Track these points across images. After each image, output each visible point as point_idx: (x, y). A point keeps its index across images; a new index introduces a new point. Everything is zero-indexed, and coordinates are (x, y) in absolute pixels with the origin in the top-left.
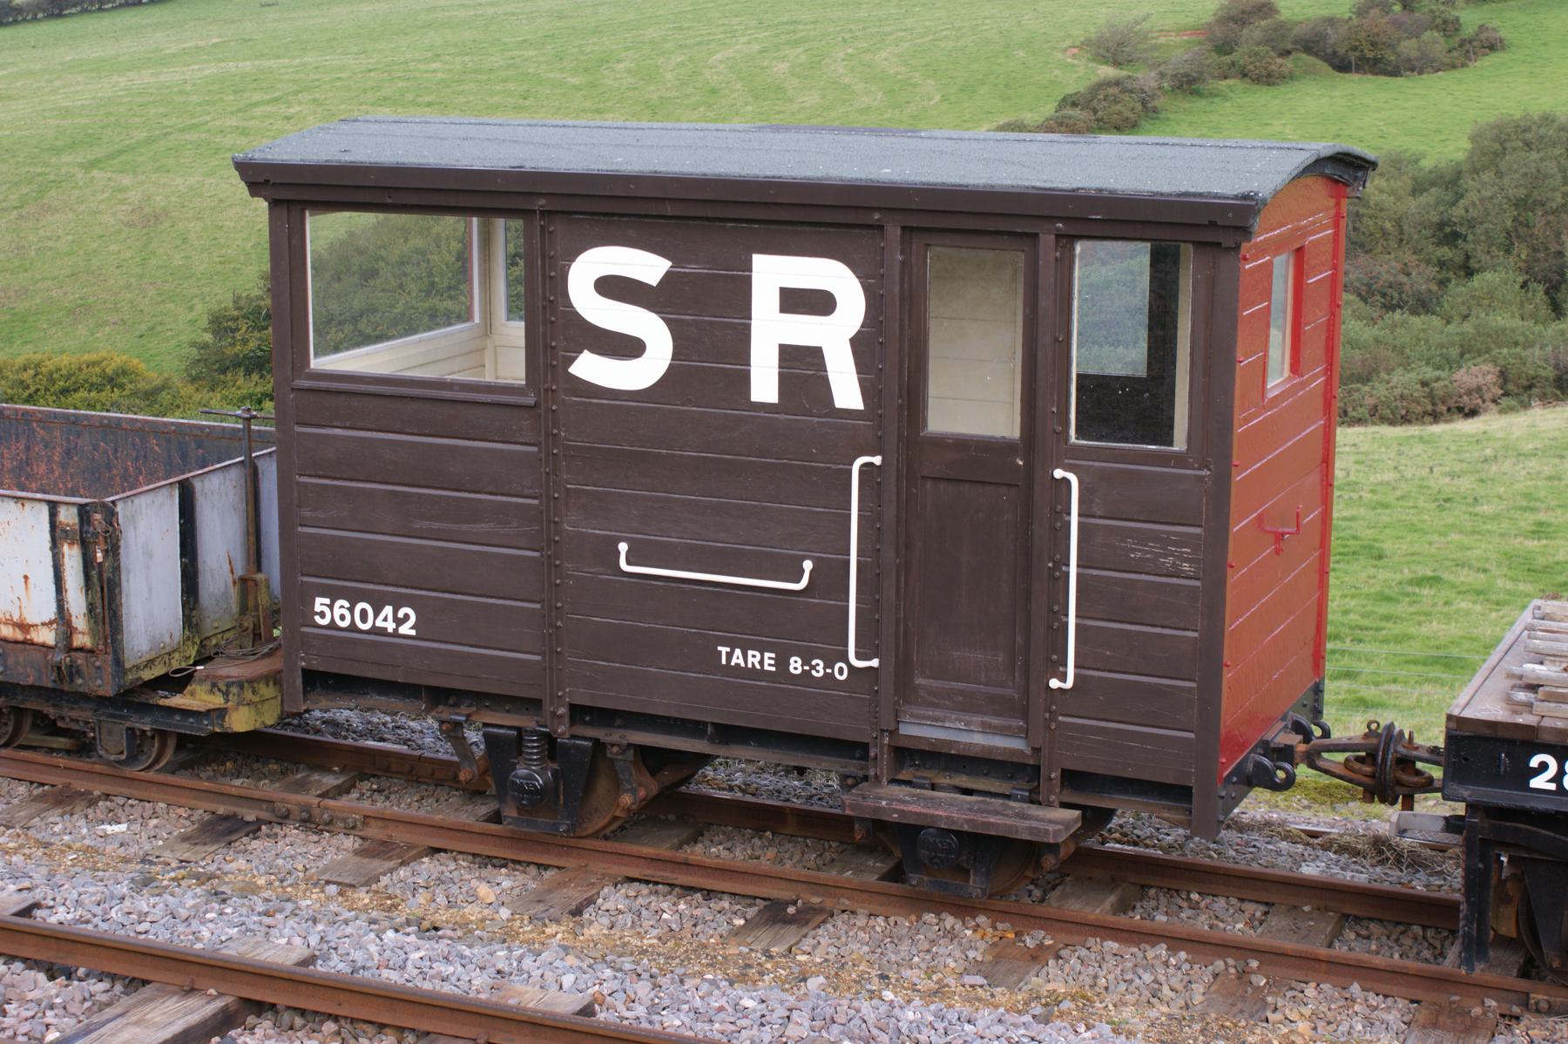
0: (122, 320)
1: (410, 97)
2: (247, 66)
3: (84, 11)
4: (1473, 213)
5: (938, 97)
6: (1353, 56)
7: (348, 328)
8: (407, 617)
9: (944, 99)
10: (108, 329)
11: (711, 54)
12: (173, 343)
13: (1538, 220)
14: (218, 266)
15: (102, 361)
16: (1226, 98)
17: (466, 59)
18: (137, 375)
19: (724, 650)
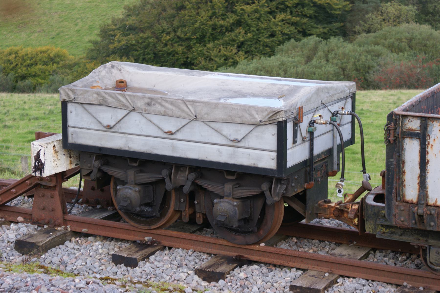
0: (43, 30)
7: (172, 35)
10: (36, 34)
12: (69, 41)
14: (88, 4)
15: (47, 51)
18: (64, 57)
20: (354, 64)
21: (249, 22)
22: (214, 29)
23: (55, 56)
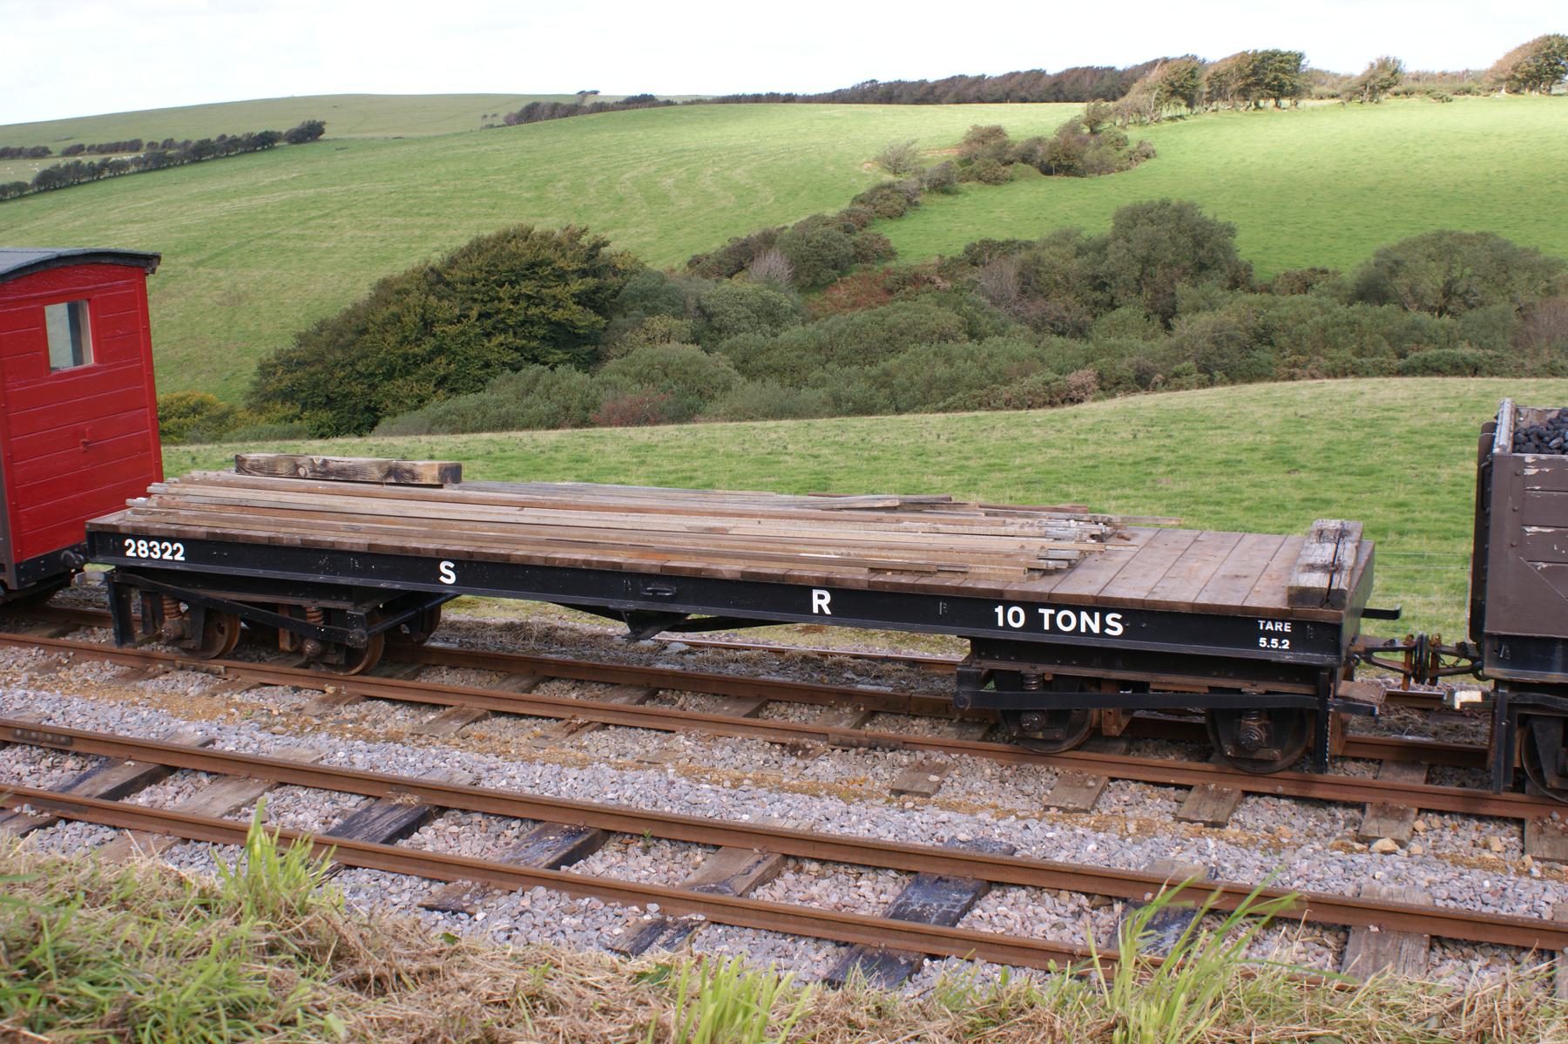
1: (416, 210)
2: (311, 192)
3: (216, 158)
4: (1112, 269)
5: (772, 199)
6: (1053, 164)
8: (178, 549)
9: (776, 200)
11: (622, 174)
13: (1158, 271)
16: (967, 195)
17: (458, 182)
19: (1262, 622)
20: (581, 401)
21: (454, 347)
22: (406, 359)
23: (197, 404)
